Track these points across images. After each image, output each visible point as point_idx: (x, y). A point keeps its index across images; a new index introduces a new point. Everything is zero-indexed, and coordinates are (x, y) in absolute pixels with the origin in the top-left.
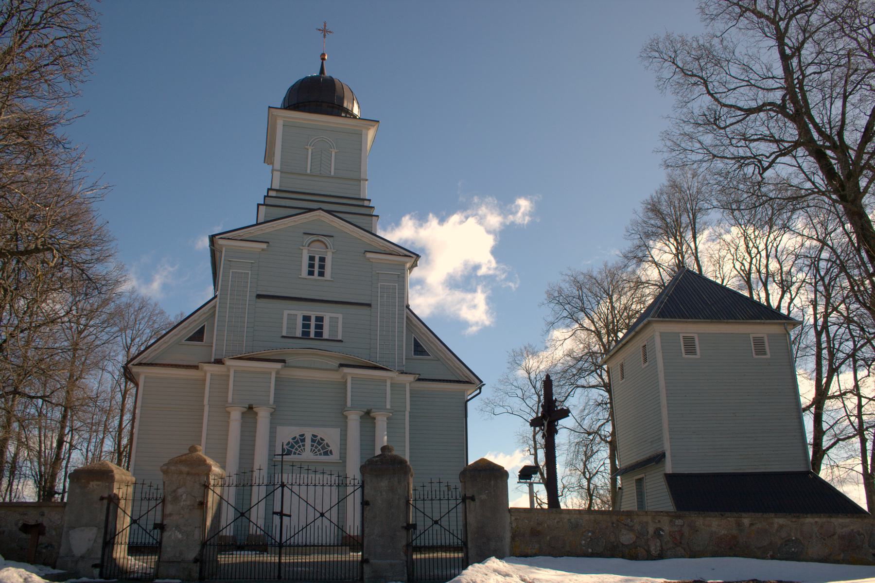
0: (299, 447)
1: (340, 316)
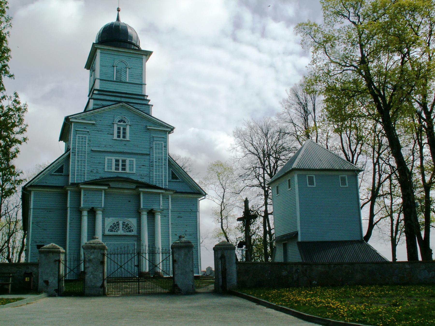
0: (126, 230)
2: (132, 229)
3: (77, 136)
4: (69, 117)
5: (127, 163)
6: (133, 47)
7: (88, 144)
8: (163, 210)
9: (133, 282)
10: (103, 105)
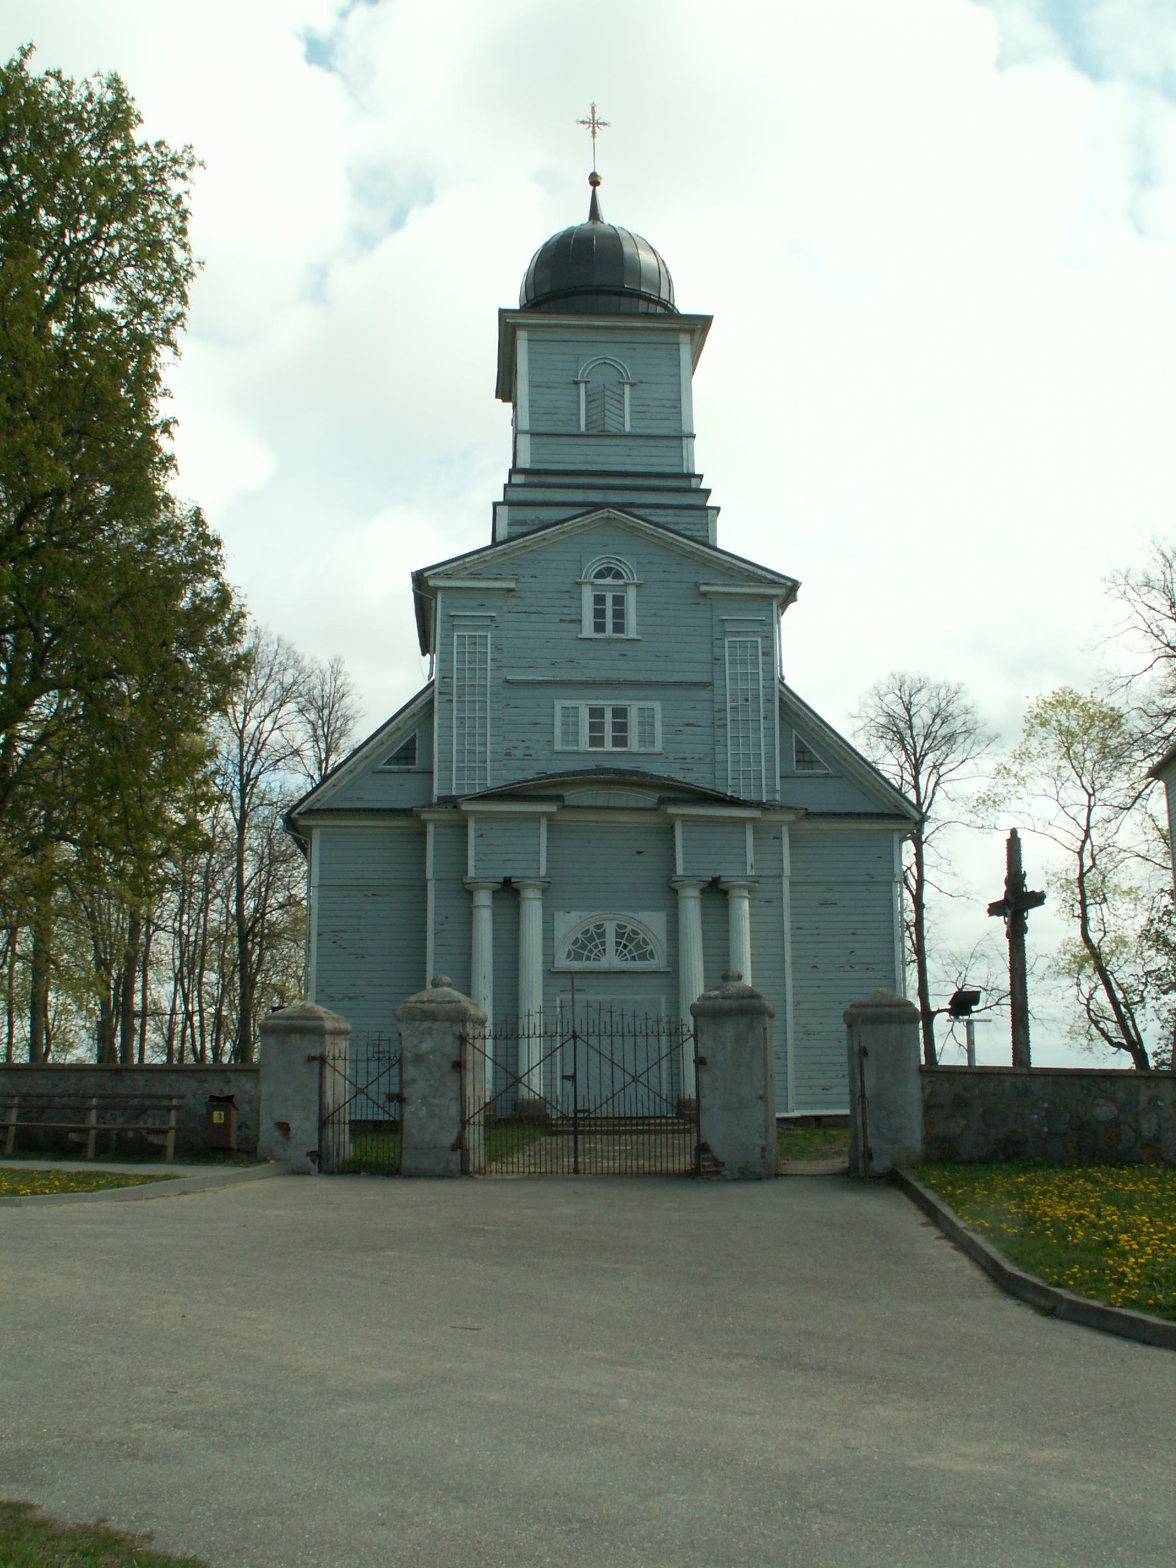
0: (596, 946)
1: (657, 706)
2: (649, 948)
3: (455, 634)
4: (426, 574)
5: (633, 719)
6: (643, 307)
7: (492, 660)
8: (756, 879)
9: (649, 1132)
10: (541, 521)
